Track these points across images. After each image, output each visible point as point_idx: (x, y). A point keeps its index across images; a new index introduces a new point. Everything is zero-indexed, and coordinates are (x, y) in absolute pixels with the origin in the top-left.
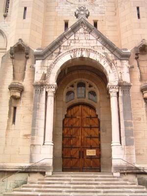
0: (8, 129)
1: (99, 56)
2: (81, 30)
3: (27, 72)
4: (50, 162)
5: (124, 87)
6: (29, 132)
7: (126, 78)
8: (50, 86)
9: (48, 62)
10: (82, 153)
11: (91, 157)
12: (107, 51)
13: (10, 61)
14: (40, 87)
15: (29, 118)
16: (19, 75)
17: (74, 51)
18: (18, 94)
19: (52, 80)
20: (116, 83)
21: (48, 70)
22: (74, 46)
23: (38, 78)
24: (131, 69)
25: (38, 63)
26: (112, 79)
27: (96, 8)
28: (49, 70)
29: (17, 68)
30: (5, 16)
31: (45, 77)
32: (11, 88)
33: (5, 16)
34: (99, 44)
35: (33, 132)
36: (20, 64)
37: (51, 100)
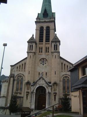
0: (26, 101)
1: (45, 85)
2: (41, 79)
3: (30, 88)
4: (34, 108)
5: (49, 93)
6: (30, 102)
7: (50, 91)
8: (34, 93)
9: (34, 87)
10: (42, 106)
11: (44, 107)
12: (46, 84)
13: (26, 86)
14: (32, 93)
15: (30, 99)
16: (28, 89)
17: (40, 84)
18: (28, 94)
19: (35, 91)
20: (48, 92)
21: (34, 89)
22: (40, 83)
23: (32, 90)
24: (51, 89)
25: (32, 87)
26: (47, 92)
27: (47, 69)
28: (34, 89)
29: (28, 87)
30: (24, 71)
31: (33, 90)
32: (27, 92)
33: (24, 71)
34: (45, 83)
35: (31, 102)
36: (28, 86)
37: (34, 95)
